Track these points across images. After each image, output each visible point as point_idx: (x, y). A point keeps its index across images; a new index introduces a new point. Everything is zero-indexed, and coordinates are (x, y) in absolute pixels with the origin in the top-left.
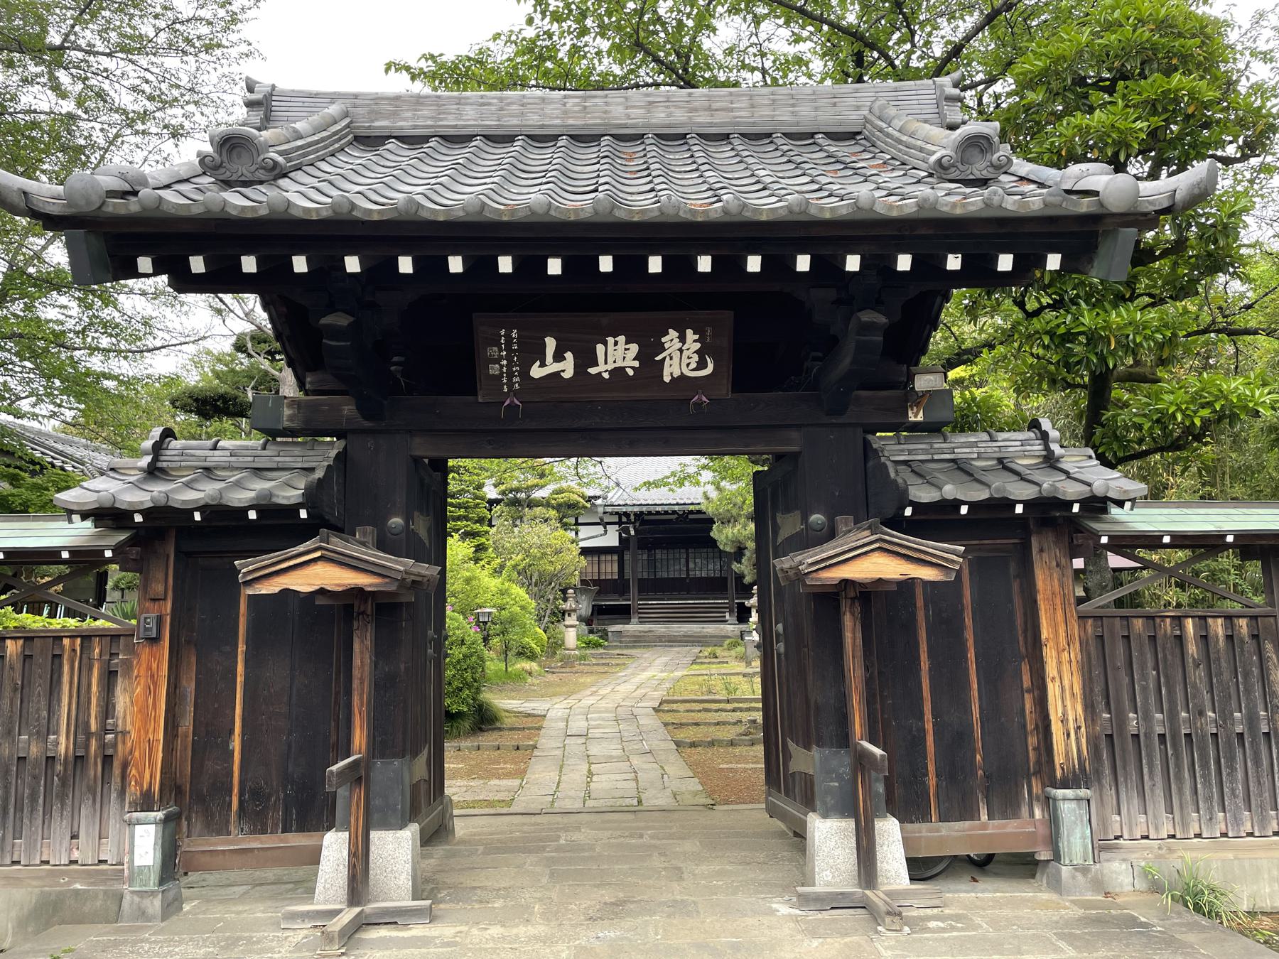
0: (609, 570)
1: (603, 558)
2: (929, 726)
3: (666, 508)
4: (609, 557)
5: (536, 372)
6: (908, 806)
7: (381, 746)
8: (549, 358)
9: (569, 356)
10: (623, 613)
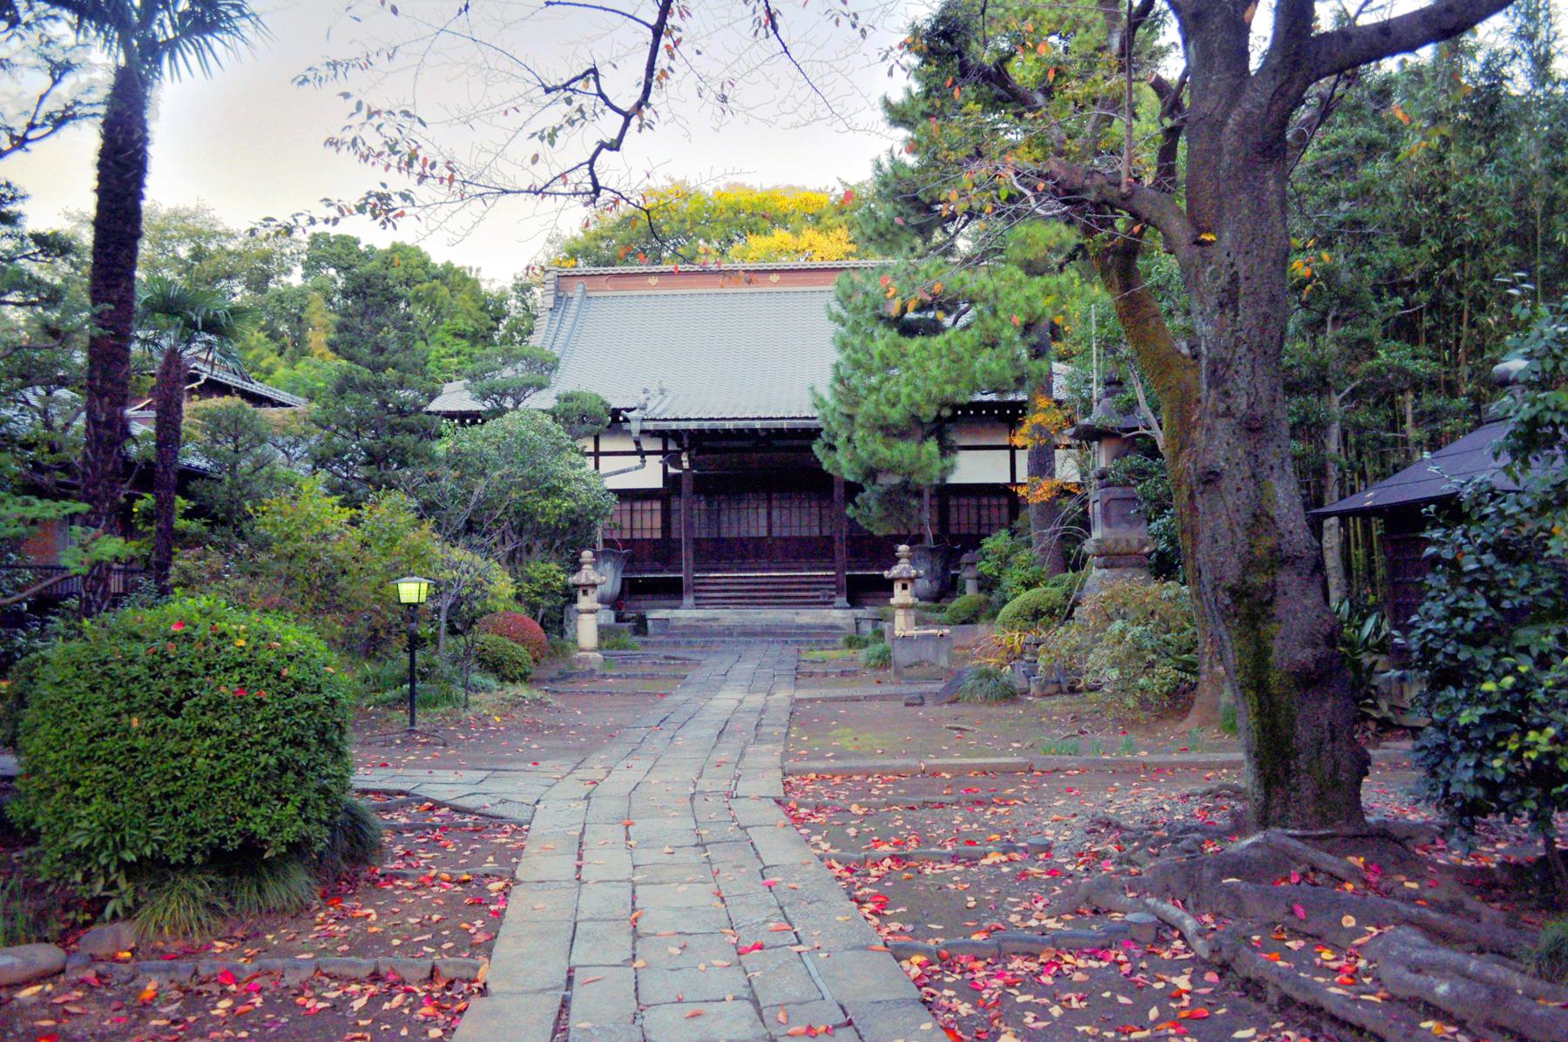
0: (647, 524)
1: (638, 505)
3: (741, 424)
4: (647, 506)
10: (672, 591)
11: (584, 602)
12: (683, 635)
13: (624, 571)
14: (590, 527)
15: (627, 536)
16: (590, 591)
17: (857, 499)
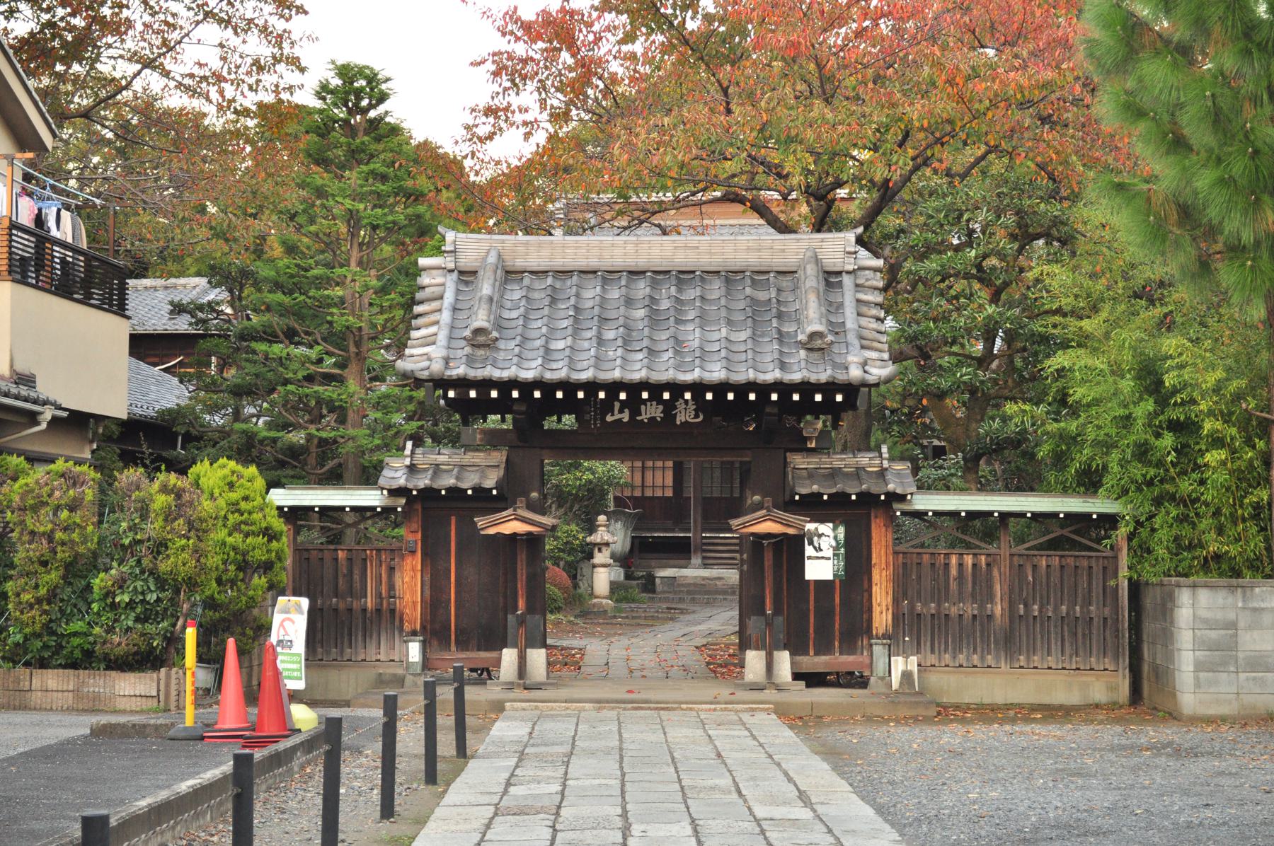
2: (812, 607)
5: (609, 418)
6: (797, 648)
7: (530, 609)
8: (616, 411)
9: (627, 411)
10: (680, 551)
11: (599, 558)
12: (689, 592)
13: (635, 530)
14: (603, 494)
15: (638, 493)
16: (604, 549)
17: (716, 419)
